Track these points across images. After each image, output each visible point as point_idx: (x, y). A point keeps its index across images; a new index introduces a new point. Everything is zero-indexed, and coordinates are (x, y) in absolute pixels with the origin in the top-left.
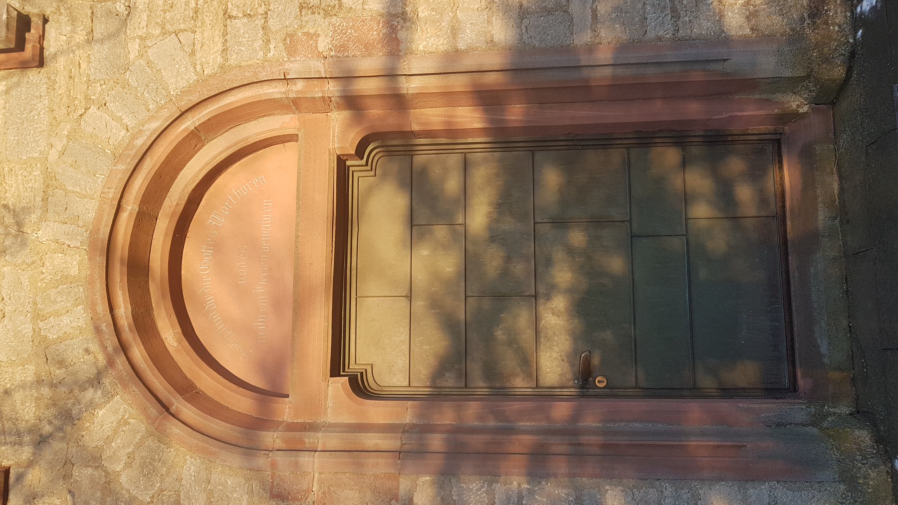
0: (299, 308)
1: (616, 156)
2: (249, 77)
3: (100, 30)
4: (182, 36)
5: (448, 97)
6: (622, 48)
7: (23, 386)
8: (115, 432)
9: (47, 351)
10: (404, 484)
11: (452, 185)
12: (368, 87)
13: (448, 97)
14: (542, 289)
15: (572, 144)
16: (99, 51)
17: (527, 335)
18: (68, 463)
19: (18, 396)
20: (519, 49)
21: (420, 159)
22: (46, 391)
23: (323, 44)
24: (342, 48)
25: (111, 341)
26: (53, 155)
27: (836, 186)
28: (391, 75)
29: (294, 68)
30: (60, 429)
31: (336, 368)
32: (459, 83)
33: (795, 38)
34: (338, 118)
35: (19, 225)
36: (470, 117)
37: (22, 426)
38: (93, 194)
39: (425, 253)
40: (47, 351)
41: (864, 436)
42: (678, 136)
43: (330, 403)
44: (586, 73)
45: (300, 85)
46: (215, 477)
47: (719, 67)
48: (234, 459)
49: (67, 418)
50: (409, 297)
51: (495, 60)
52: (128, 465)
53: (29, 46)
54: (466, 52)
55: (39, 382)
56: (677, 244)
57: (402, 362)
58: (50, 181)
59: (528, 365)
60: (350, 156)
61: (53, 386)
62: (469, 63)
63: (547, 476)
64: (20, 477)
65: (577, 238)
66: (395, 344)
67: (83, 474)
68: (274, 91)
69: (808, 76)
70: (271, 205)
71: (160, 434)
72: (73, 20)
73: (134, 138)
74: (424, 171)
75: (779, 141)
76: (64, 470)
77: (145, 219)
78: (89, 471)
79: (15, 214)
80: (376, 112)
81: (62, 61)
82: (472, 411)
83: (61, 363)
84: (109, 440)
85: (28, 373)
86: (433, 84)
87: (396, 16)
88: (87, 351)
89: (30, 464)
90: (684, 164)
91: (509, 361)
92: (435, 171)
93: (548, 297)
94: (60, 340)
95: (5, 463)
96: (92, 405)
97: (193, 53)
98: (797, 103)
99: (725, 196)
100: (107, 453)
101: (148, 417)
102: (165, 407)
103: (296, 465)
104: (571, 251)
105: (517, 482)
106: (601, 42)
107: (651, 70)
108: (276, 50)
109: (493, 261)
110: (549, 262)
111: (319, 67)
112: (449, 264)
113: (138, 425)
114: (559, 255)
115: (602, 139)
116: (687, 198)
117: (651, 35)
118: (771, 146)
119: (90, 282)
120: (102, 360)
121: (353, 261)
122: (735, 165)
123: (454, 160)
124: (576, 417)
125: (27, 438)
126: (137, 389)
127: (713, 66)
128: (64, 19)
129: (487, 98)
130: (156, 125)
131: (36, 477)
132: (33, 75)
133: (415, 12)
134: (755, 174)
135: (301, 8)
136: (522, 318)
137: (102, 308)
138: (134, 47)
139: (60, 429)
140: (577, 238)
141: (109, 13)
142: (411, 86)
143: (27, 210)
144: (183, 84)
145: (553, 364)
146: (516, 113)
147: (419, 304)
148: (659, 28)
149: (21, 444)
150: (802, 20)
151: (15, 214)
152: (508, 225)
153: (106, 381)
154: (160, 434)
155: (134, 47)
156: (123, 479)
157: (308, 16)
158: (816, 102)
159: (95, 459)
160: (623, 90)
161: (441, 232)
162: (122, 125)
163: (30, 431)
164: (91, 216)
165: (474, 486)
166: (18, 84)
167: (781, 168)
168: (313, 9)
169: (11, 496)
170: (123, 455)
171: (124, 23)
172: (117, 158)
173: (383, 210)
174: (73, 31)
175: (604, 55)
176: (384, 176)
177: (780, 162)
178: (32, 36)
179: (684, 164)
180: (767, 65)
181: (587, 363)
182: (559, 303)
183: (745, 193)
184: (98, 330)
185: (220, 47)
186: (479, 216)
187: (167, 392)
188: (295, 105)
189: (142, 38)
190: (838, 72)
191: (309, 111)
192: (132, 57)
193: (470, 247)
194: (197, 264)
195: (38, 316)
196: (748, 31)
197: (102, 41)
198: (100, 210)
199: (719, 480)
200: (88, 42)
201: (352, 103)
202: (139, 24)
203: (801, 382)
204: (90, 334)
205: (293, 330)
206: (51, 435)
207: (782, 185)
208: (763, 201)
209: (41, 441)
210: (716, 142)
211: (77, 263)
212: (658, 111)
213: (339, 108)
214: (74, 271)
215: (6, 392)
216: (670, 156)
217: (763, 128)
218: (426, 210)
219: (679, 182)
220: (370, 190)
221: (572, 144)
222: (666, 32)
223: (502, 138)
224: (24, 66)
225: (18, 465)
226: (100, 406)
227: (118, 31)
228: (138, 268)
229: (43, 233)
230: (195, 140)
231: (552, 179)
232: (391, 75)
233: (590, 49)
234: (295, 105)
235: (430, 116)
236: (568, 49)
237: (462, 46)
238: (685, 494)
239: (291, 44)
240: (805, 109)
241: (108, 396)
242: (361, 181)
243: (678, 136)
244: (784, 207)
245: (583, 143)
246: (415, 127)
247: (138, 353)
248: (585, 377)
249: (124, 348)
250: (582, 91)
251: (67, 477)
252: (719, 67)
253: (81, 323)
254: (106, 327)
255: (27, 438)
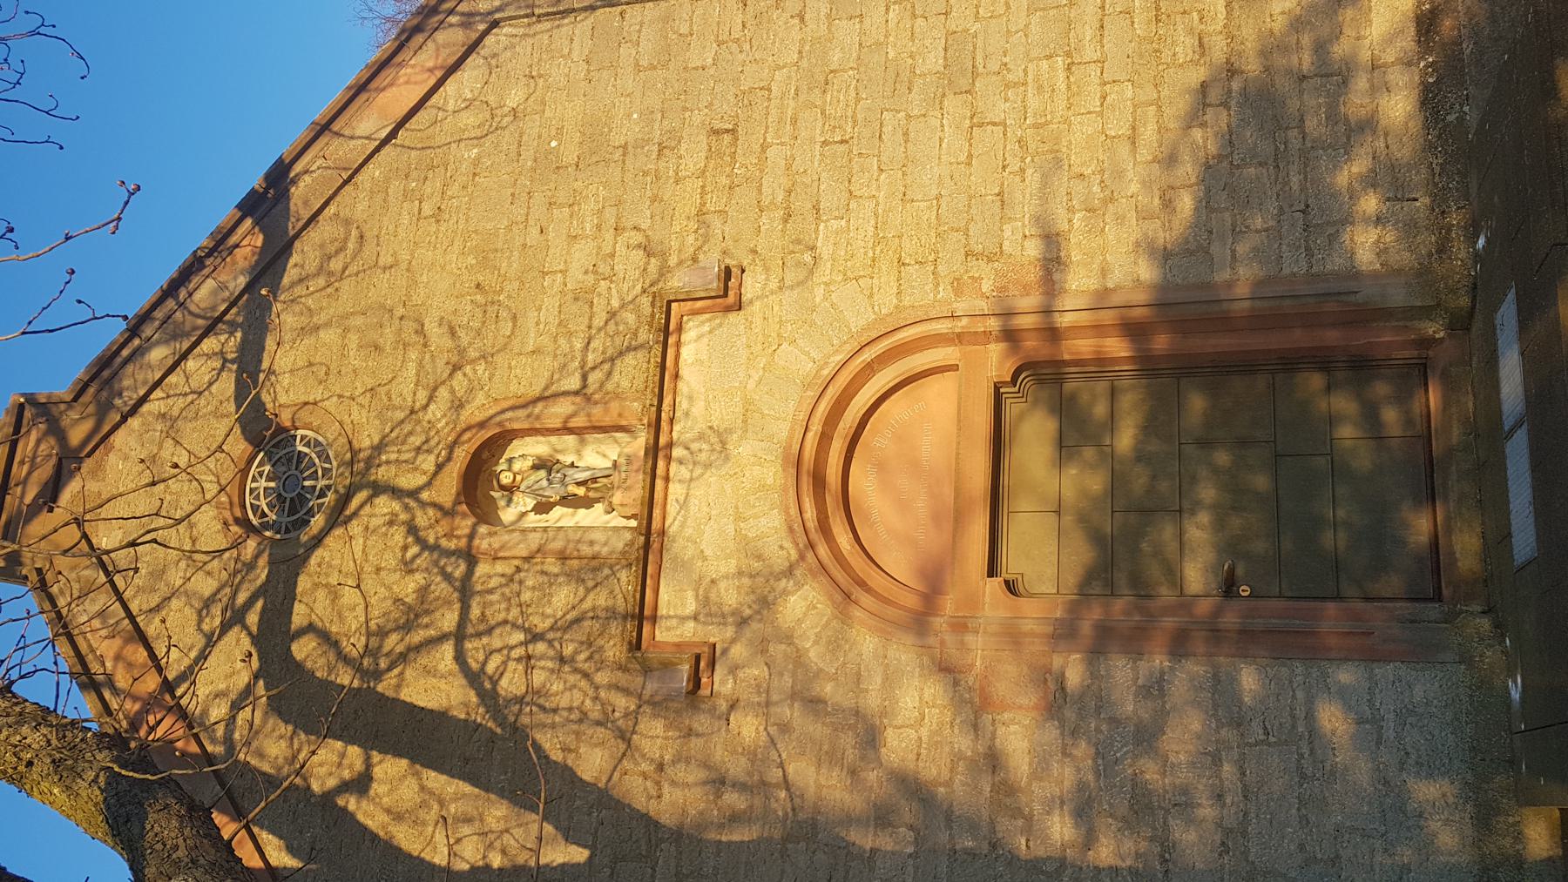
0: (959, 517)
1: (1261, 381)
2: (921, 315)
3: (790, 278)
4: (861, 281)
5: (1098, 329)
6: (1259, 284)
7: (726, 577)
8: (805, 615)
9: (749, 548)
10: (1057, 661)
11: (1100, 410)
12: (1026, 322)
13: (1098, 329)
14: (1186, 505)
15: (1216, 371)
16: (789, 297)
17: (1172, 547)
18: (764, 641)
19: (722, 585)
20: (1163, 287)
21: (1069, 387)
22: (746, 581)
23: (986, 286)
24: (1003, 289)
25: (802, 540)
26: (751, 384)
27: (1471, 405)
28: (1047, 311)
29: (961, 307)
30: (758, 612)
31: (992, 571)
32: (1108, 317)
33: (1423, 273)
34: (996, 349)
35: (723, 443)
36: (1117, 347)
37: (726, 609)
38: (785, 416)
39: (1074, 472)
40: (749, 548)
41: (1485, 624)
42: (1323, 361)
43: (987, 599)
44: (1225, 306)
45: (965, 321)
46: (890, 653)
47: (1352, 298)
48: (909, 639)
49: (766, 604)
50: (1058, 512)
51: (1141, 297)
52: (816, 643)
53: (731, 293)
54: (1114, 290)
55: (740, 573)
56: (1321, 462)
57: (1051, 571)
58: (748, 407)
59: (1174, 576)
60: (1005, 384)
61: (751, 576)
62: (1117, 299)
63: (1186, 655)
64: (725, 651)
65: (1222, 458)
66: (1044, 554)
67: (777, 650)
68: (942, 327)
69: (1438, 305)
70: (936, 424)
71: (843, 616)
72: (767, 269)
73: (822, 368)
74: (1073, 398)
75: (1425, 366)
76: (761, 647)
77: (825, 438)
78: (783, 647)
79: (719, 434)
80: (1031, 344)
81: (757, 304)
82: (1119, 605)
83: (759, 557)
84: (799, 621)
85: (731, 566)
86: (1084, 318)
87: (1051, 260)
88: (781, 547)
89: (733, 641)
90: (1329, 389)
91: (1154, 571)
92: (1084, 398)
93: (1193, 513)
94: (758, 538)
95: (712, 640)
96: (785, 592)
97: (871, 295)
98: (1434, 329)
99: (1370, 417)
100: (798, 633)
101: (834, 603)
102: (848, 596)
103: (962, 643)
104: (1216, 470)
105: (1160, 660)
106: (1240, 277)
107: (1288, 302)
108: (944, 292)
109: (1140, 480)
110: (1194, 479)
111: (983, 306)
112: (1096, 483)
113: (825, 609)
114: (1203, 472)
115: (1243, 365)
116: (1332, 420)
117: (1286, 271)
118: (1419, 371)
119: (785, 490)
120: (794, 555)
121: (1005, 480)
122: (1381, 389)
123: (1102, 387)
124: (1217, 613)
125: (730, 620)
126: (824, 579)
127: (1344, 298)
128: (759, 269)
129: (1133, 330)
130: (840, 358)
131: (738, 651)
132: (733, 317)
133: (1069, 256)
134: (1402, 398)
135: (967, 255)
136: (1168, 532)
137: (794, 511)
138: (819, 292)
139: (758, 612)
140: (1222, 458)
141: (798, 264)
142: (1064, 320)
143: (729, 431)
144: (862, 322)
145: (1196, 575)
146: (1161, 343)
147: (1068, 519)
148: (1294, 265)
149: (725, 624)
150: (1430, 255)
151: (719, 434)
152: (1154, 446)
153: (798, 573)
154: (843, 616)
155: (819, 292)
156: (812, 654)
157: (972, 262)
158: (1451, 327)
159: (788, 638)
160: (1260, 321)
161: (1089, 453)
162: (808, 357)
163: (733, 614)
164: (785, 434)
165: (1120, 663)
166: (720, 325)
167: (1427, 391)
168: (977, 256)
169: (717, 667)
170: (811, 634)
171: (811, 272)
172: (806, 386)
173: (1034, 435)
174: (767, 279)
175: (1242, 290)
176: (1036, 402)
177: (1426, 385)
178: (733, 282)
179: (1329, 389)
180: (1398, 297)
181: (1232, 571)
182: (1204, 517)
183: (1390, 416)
184: (791, 530)
185: (895, 290)
186: (1125, 439)
187: (848, 588)
188: (959, 338)
189: (826, 284)
190: (1464, 301)
191: (970, 344)
192: (818, 300)
193: (1117, 467)
194: (863, 481)
195: (739, 518)
196: (1378, 266)
197: (792, 288)
198: (792, 429)
199: (1346, 659)
200: (780, 288)
201: (1010, 336)
202: (825, 272)
203: (1445, 592)
204: (784, 533)
205: (954, 537)
206: (750, 617)
207: (1428, 407)
208: (1409, 422)
209: (743, 622)
210: (1359, 368)
211: (773, 474)
212: (1298, 338)
213: (998, 340)
214: (770, 481)
215: (713, 581)
216: (1316, 381)
217: (1407, 354)
218: (1075, 435)
219: (1324, 405)
220: (1021, 417)
221: (1216, 371)
222: (1301, 268)
223: (1147, 366)
224: (728, 309)
225: (723, 641)
226: (792, 593)
227: (807, 279)
228: (819, 481)
229: (743, 449)
230: (869, 370)
231: (1197, 404)
232: (1047, 311)
233: (1230, 285)
234: (959, 338)
235: (1083, 346)
236: (1208, 286)
237: (1110, 285)
238: (1315, 672)
239: (958, 287)
240: (1442, 334)
241: (799, 586)
242: (1012, 408)
243: (1323, 361)
244: (1429, 427)
245: (369, 122)
246: (1066, 357)
247: (823, 550)
248: (1229, 588)
249: (812, 546)
250: (1223, 322)
251: (764, 652)
252: (1352, 298)
253: (777, 523)
254: (797, 527)
255: (730, 620)
